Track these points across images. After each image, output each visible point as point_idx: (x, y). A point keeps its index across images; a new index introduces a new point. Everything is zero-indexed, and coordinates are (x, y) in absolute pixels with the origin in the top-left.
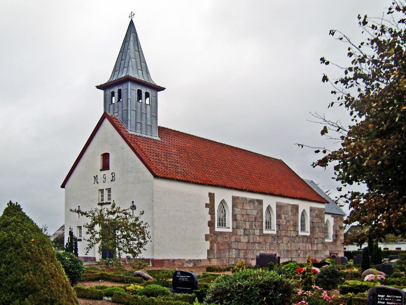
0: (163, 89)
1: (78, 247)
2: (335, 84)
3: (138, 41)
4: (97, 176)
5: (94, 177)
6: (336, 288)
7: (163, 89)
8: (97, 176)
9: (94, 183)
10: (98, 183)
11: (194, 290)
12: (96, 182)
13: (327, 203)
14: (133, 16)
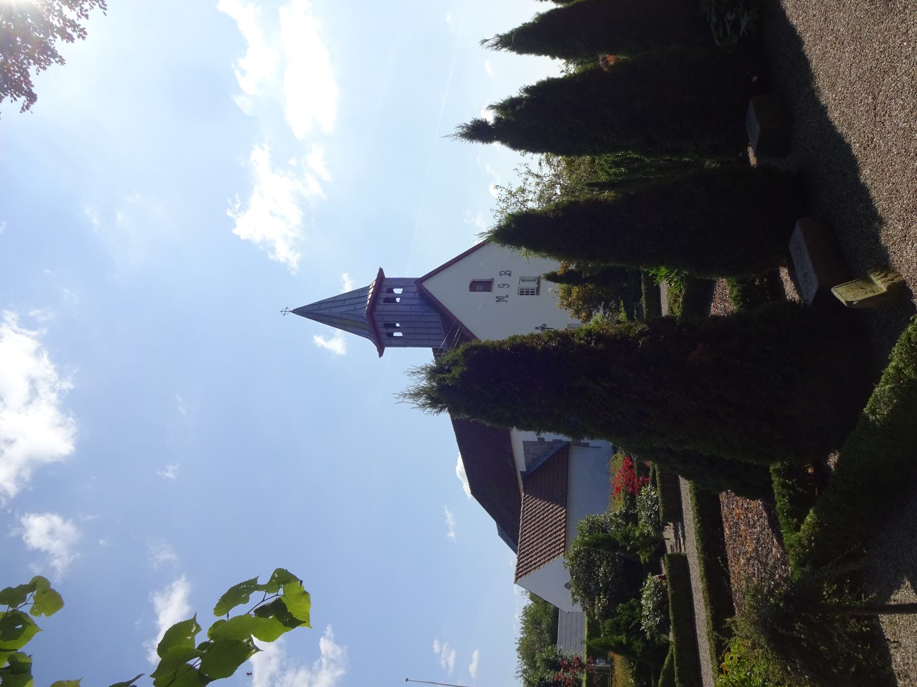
0: (381, 271)
1: (548, 57)
2: (85, 39)
3: (330, 300)
4: (497, 297)
5: (497, 301)
6: (621, 312)
7: (381, 271)
8: (497, 297)
9: (507, 301)
10: (507, 296)
11: (641, 267)
12: (505, 299)
13: (257, 589)
14: (286, 313)
